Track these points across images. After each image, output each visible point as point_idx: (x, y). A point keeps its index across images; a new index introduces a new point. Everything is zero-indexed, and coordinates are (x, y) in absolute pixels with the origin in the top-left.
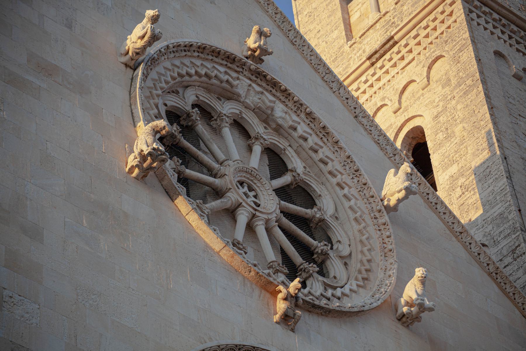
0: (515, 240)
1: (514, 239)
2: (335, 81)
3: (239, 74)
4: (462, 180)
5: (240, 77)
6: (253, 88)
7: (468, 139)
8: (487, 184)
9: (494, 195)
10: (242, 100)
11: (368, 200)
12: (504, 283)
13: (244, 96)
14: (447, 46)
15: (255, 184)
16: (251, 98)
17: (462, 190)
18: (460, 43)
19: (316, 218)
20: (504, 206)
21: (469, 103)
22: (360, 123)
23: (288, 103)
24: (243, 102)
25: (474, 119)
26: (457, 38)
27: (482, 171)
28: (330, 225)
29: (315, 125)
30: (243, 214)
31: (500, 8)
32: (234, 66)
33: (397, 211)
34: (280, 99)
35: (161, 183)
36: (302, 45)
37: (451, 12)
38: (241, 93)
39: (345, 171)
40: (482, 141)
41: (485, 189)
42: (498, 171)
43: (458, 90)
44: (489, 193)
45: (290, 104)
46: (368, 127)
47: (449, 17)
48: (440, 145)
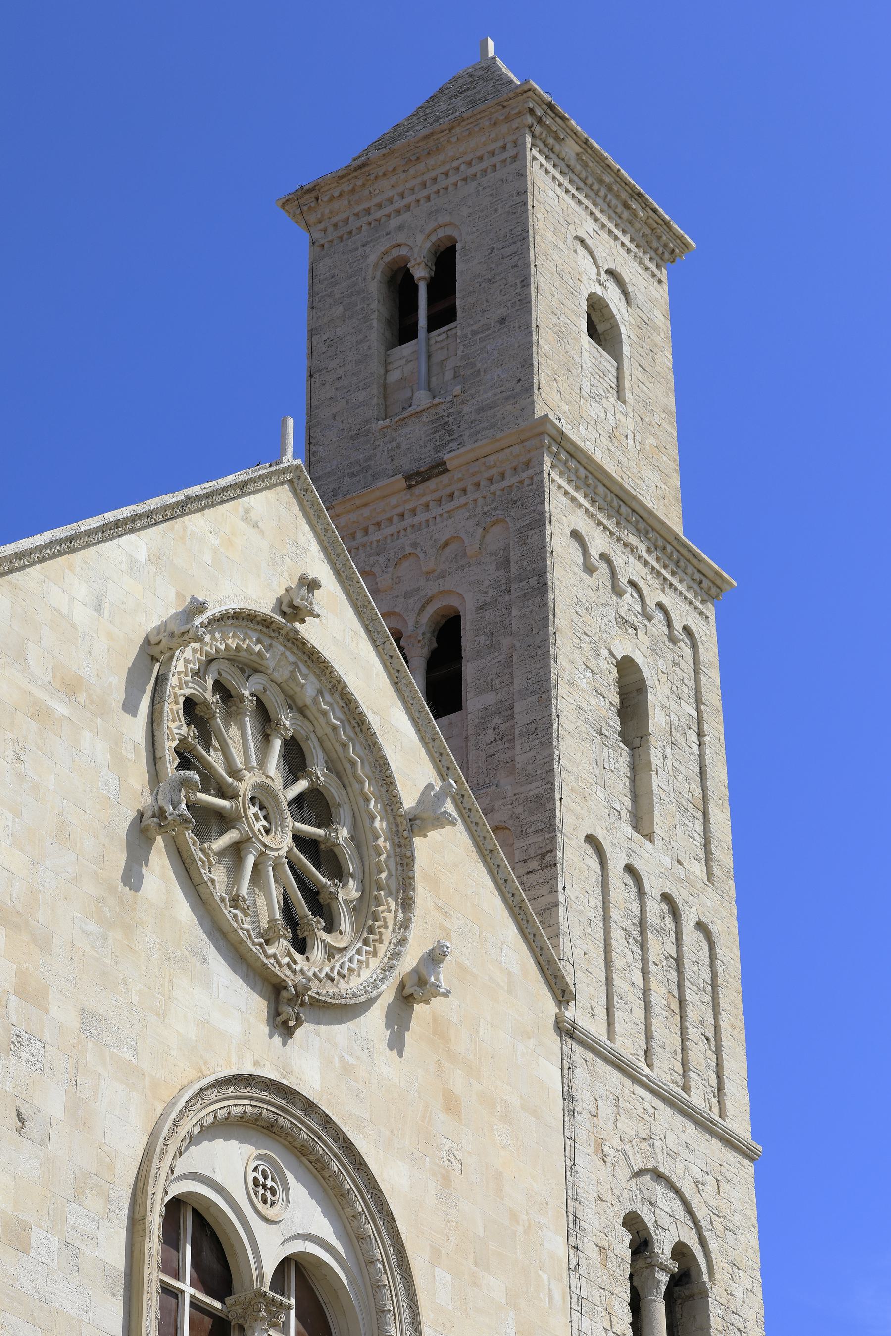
5: (275, 643)
8: (528, 744)
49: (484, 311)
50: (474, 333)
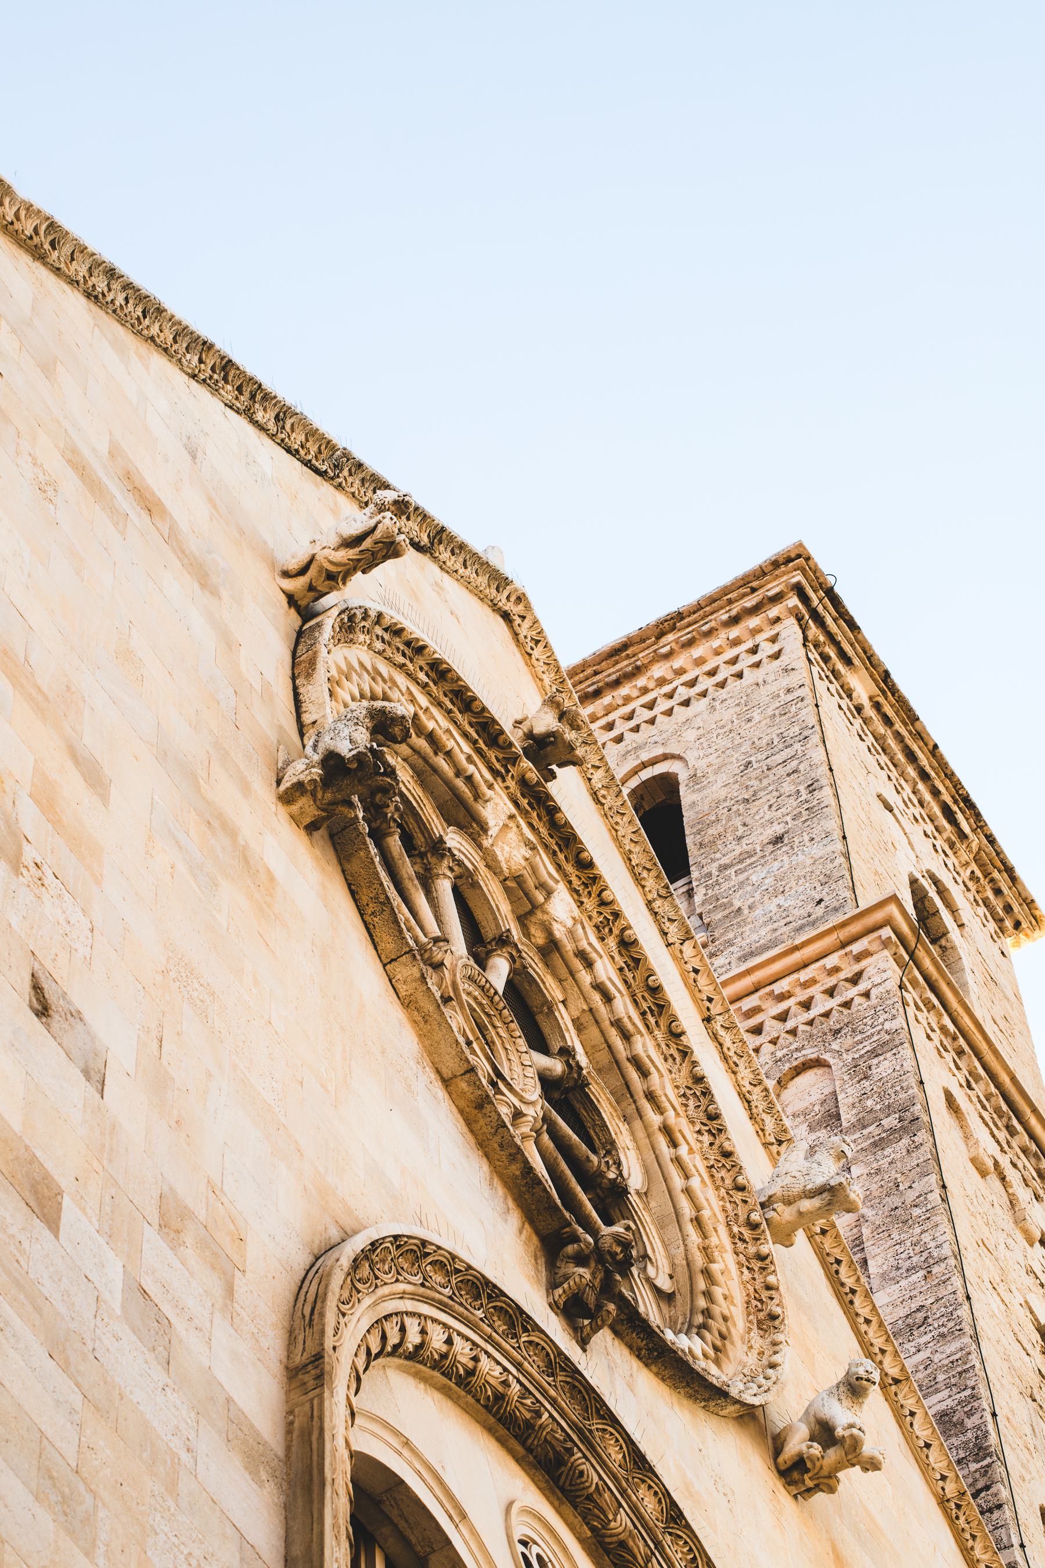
0: (977, 1475)
1: (975, 1472)
2: (676, 920)
3: (495, 779)
7: (872, 1243)
8: (912, 1344)
9: (929, 1371)
10: (486, 843)
11: (728, 1193)
12: (971, 1534)
13: (494, 835)
14: (839, 1041)
15: (495, 1027)
16: (507, 849)
18: (875, 1038)
19: (605, 1181)
20: (958, 1396)
21: (886, 1165)
22: (715, 1037)
23: (585, 900)
25: (896, 1201)
26: (869, 1028)
27: (902, 1315)
29: (634, 977)
31: (960, 1010)
32: (492, 754)
33: (792, 1245)
34: (570, 882)
35: (341, 865)
36: (618, 812)
37: (856, 974)
38: (491, 823)
39: (684, 1108)
40: (911, 1251)
41: (907, 1355)
42: (949, 1320)
43: (857, 1135)
44: (916, 1366)
45: (590, 904)
46: (731, 1053)
47: (848, 985)
49: (740, 838)
50: (726, 867)
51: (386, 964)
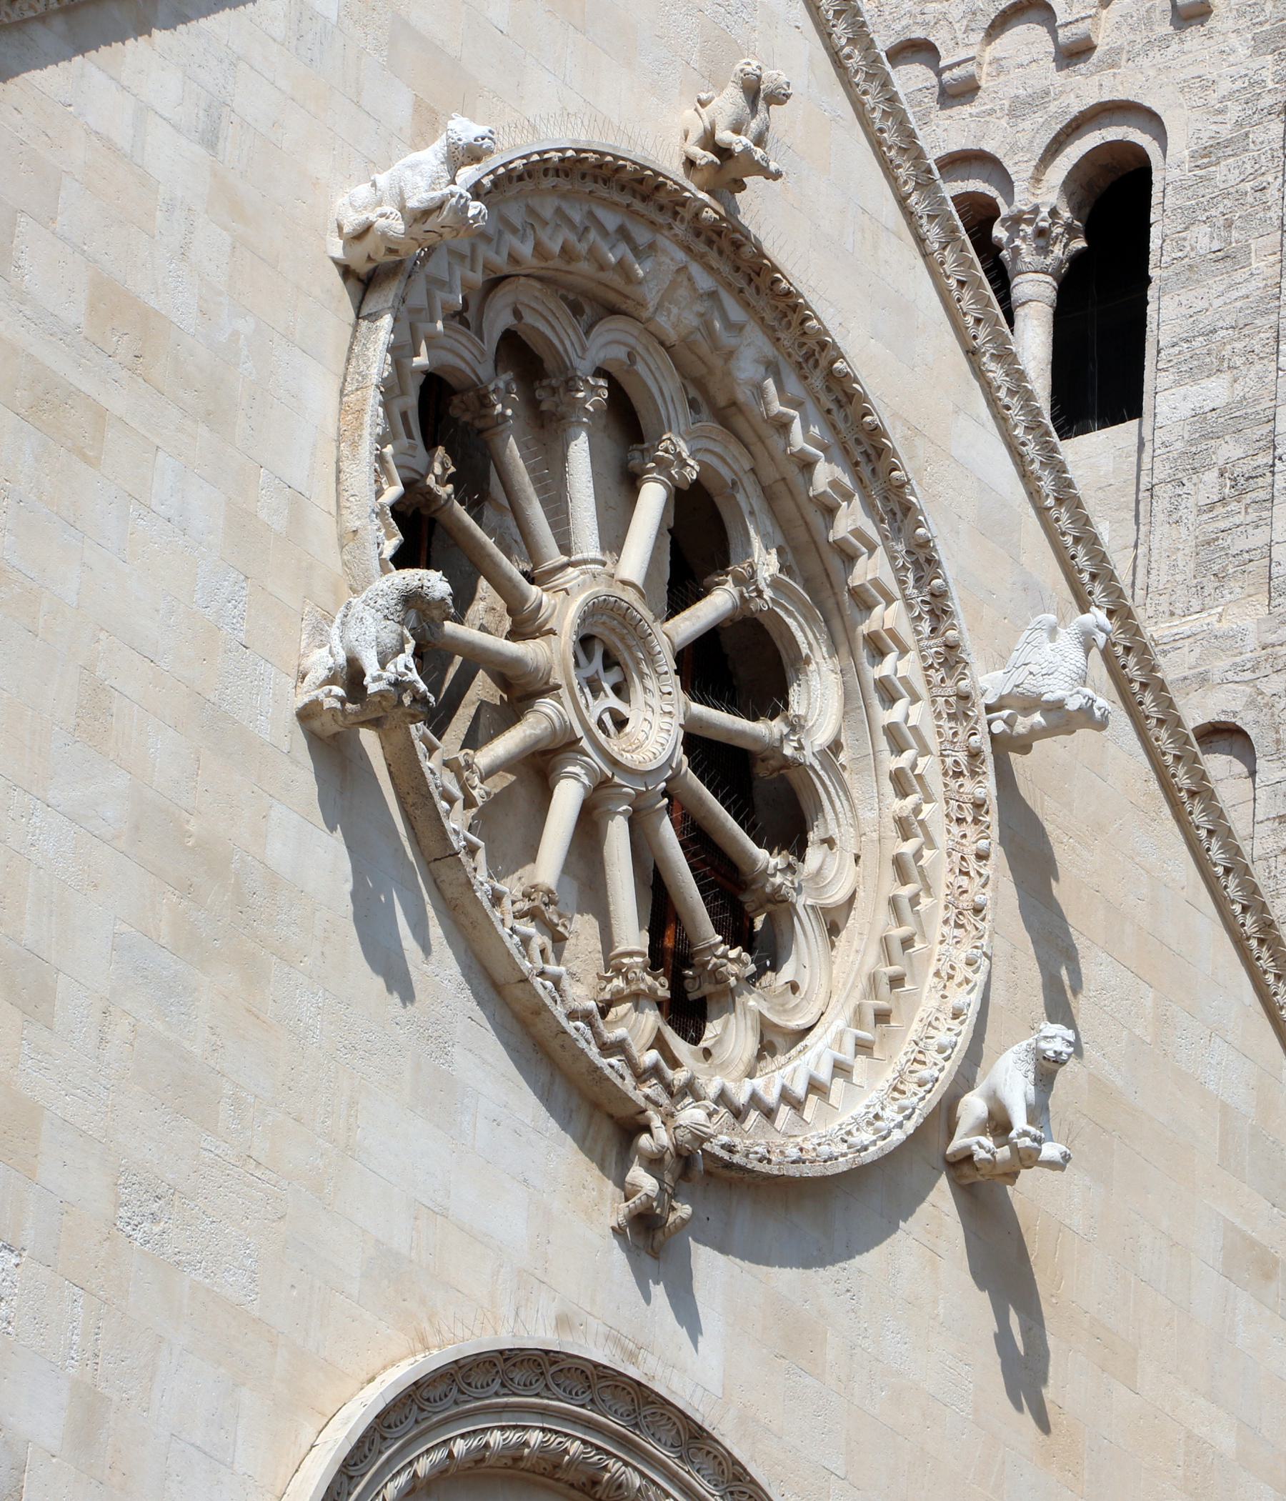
4: (1229, 450)
6: (690, 279)
17: (1223, 486)
24: (649, 320)
28: (821, 790)
30: (575, 777)
48: (1190, 272)
51: (429, 863)
